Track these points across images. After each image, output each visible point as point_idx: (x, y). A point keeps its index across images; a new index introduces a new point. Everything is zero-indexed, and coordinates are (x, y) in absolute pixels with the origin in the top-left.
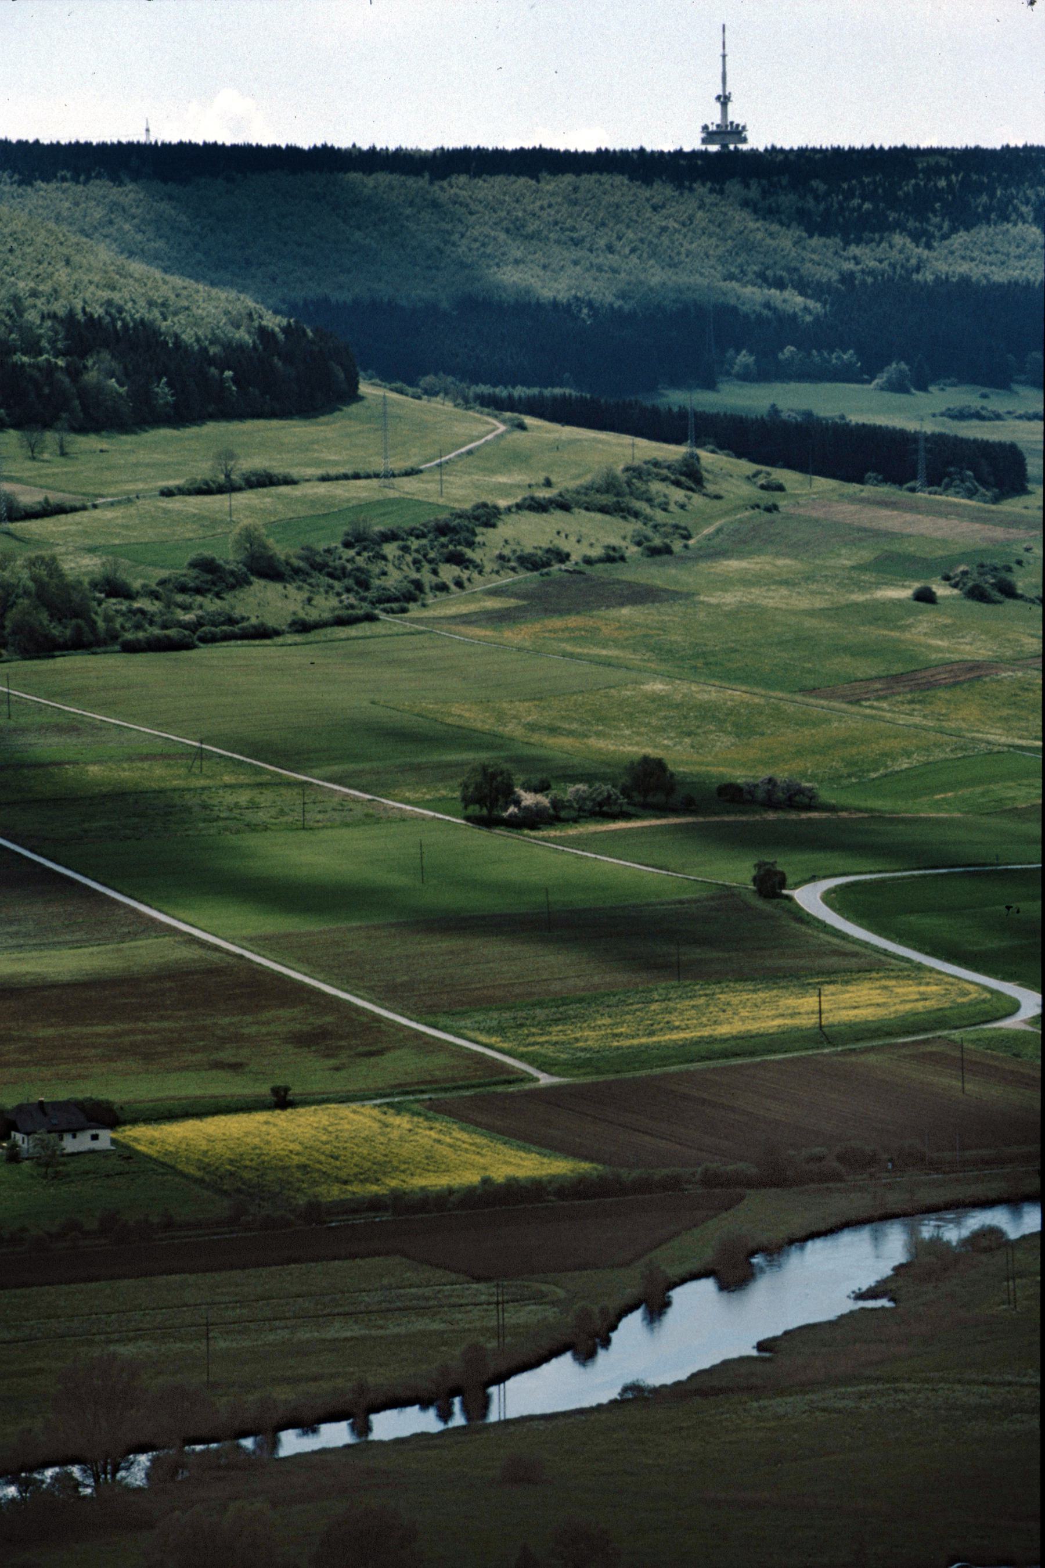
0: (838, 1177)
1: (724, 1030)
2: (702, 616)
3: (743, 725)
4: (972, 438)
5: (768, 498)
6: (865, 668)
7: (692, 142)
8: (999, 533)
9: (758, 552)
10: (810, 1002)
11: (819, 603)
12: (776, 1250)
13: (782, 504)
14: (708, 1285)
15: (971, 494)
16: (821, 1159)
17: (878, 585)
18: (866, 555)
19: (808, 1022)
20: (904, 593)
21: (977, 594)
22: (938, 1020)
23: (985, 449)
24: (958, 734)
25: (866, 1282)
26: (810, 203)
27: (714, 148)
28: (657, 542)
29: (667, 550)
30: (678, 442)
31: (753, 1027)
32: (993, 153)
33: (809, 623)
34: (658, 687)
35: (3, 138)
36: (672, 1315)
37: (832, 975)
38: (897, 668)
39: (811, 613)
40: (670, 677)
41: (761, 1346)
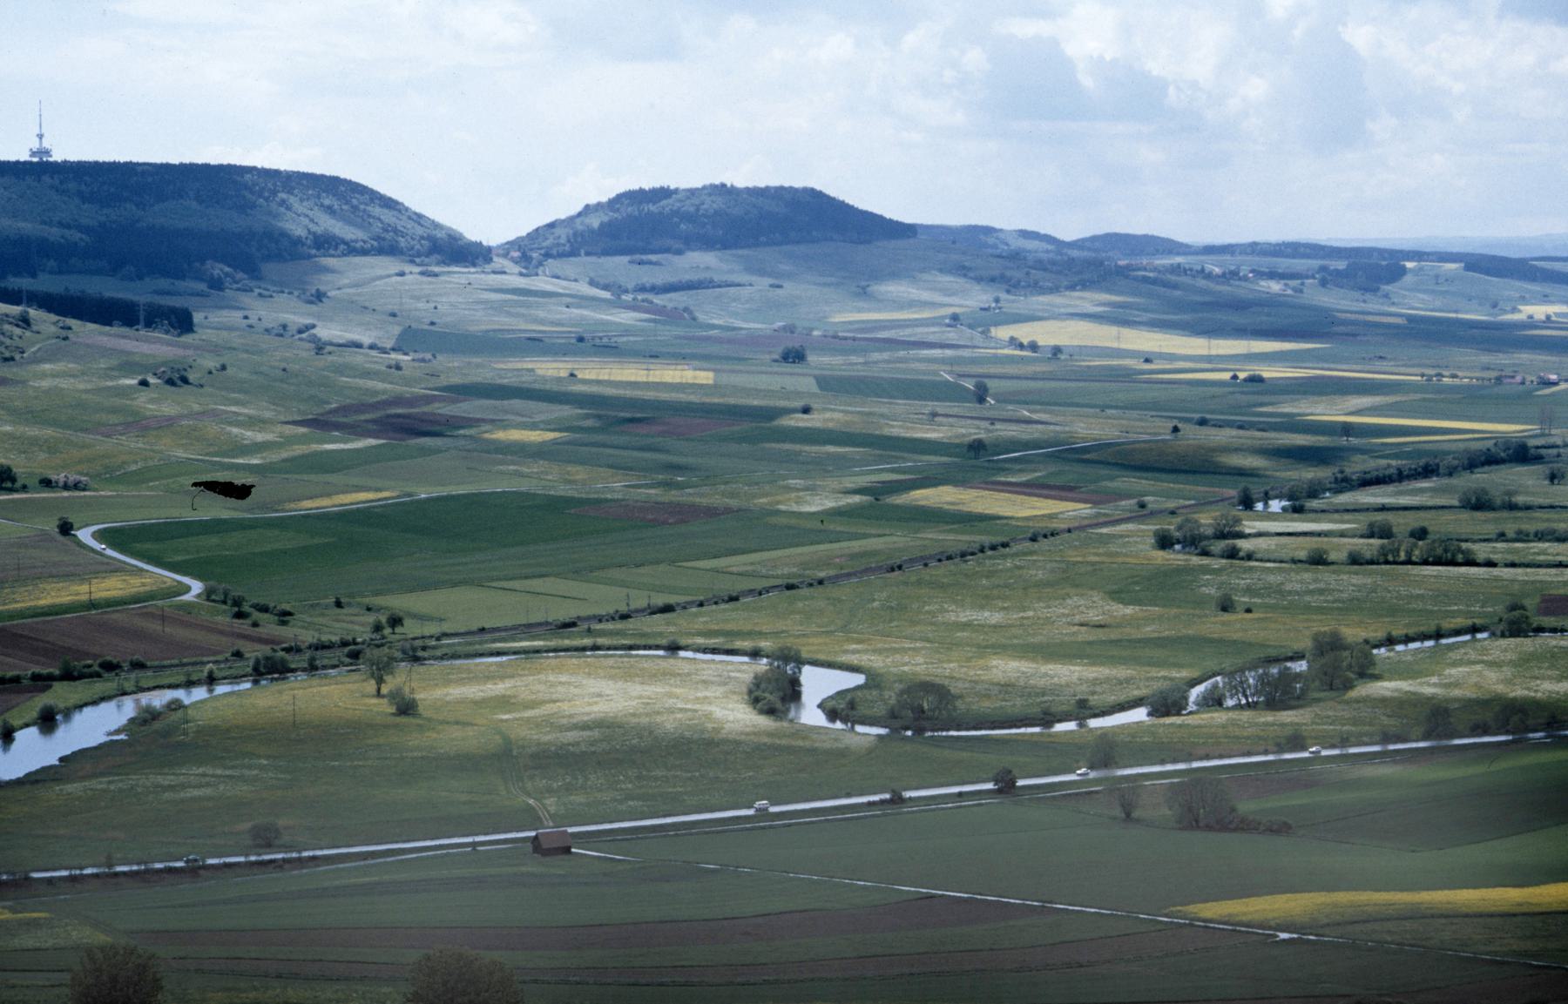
0: (99, 675)
1: (42, 602)
2: (30, 392)
3: (51, 448)
4: (147, 279)
5: (64, 333)
6: (113, 419)
7: (24, 157)
8: (180, 352)
9: (59, 360)
10: (85, 588)
11: (89, 386)
12: (68, 714)
13: (71, 336)
14: (34, 730)
15: (167, 332)
16: (90, 666)
17: (119, 377)
18: (114, 362)
19: (85, 598)
20: (134, 382)
21: (170, 382)
22: (151, 596)
23: (173, 311)
24: (161, 452)
25: (114, 727)
26: (83, 187)
27: (35, 160)
28: (7, 355)
29: (12, 359)
30: (18, 303)
31: (58, 601)
32: (174, 166)
33: (84, 396)
34: (8, 428)
35: (17, 151)
36: (15, 746)
37: (96, 574)
38: (130, 419)
39: (87, 391)
40: (13, 423)
41: (61, 759)
